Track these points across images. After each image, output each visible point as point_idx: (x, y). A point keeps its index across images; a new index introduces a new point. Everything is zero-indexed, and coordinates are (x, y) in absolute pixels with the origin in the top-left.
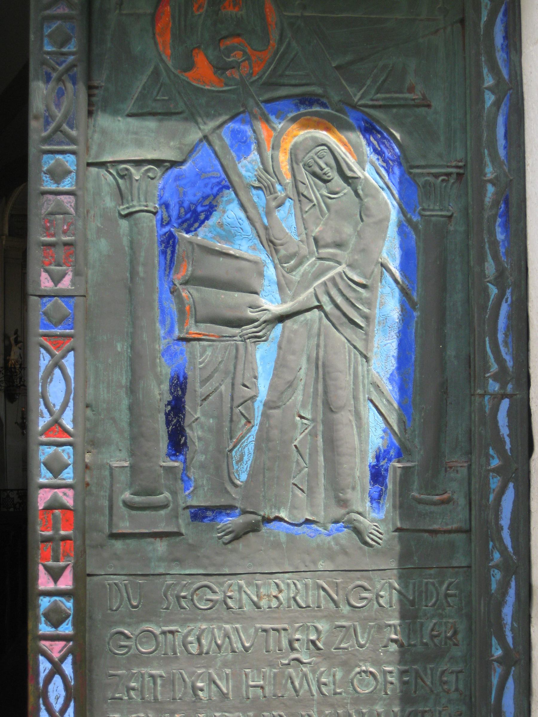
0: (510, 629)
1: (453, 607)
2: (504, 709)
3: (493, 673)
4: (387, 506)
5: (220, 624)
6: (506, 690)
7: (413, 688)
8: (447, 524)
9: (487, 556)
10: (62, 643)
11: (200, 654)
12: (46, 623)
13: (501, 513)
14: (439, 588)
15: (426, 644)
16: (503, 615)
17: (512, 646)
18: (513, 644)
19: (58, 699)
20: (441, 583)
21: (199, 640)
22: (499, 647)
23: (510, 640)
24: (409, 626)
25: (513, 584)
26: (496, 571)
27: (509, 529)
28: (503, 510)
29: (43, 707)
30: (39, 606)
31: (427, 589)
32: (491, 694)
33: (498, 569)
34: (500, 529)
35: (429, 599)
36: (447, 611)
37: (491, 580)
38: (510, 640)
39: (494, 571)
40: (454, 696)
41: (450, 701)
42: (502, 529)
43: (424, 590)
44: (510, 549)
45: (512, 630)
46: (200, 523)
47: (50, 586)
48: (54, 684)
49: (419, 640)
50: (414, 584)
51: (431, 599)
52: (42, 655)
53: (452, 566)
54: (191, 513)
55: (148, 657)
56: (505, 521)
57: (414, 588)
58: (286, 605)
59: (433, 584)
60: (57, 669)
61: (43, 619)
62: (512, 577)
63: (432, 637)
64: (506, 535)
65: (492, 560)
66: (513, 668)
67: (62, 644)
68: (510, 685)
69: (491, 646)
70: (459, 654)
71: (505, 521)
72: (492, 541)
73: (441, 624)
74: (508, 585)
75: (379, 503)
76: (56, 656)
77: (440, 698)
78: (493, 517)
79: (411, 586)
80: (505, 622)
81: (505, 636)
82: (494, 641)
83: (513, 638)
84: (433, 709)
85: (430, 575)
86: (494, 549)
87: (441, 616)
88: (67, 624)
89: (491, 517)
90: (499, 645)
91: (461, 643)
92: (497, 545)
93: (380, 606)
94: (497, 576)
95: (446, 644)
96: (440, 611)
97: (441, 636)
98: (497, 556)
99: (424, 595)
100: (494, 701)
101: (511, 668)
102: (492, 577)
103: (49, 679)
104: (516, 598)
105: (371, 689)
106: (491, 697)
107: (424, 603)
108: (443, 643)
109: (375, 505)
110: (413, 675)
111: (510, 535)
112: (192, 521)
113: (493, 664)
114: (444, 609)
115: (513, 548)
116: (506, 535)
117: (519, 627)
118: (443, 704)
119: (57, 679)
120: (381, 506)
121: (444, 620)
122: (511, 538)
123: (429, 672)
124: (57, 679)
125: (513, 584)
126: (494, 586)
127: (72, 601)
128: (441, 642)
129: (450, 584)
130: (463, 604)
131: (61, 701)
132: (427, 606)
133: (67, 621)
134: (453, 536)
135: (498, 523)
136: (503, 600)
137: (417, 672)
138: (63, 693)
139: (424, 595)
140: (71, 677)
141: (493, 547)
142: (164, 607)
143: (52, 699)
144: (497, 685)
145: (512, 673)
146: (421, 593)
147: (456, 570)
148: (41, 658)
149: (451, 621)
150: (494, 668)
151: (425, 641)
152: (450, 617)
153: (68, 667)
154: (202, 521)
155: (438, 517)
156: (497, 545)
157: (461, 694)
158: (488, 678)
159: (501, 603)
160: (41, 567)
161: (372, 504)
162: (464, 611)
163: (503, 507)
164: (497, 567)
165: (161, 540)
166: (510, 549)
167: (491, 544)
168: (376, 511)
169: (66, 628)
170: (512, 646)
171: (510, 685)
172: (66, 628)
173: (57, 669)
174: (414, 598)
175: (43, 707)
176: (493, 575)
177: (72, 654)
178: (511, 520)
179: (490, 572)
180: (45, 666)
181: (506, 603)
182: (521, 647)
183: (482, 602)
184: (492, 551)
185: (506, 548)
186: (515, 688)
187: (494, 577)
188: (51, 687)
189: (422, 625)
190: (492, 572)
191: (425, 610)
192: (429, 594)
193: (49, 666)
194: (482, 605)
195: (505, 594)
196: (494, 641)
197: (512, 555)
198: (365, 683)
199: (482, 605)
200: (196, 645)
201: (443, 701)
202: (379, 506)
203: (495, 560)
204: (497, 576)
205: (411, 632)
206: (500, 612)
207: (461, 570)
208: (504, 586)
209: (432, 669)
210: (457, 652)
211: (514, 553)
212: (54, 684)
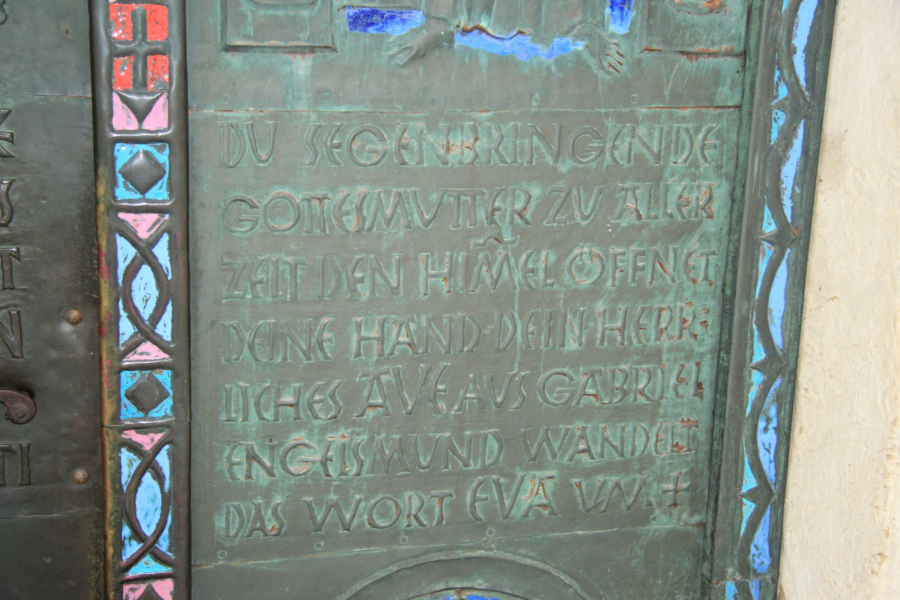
0: (789, 196)
1: (709, 163)
2: (771, 305)
3: (761, 257)
4: (634, 14)
5: (388, 188)
6: (776, 280)
7: (649, 277)
8: (713, 44)
9: (770, 91)
10: (154, 217)
11: (359, 231)
12: (126, 187)
13: (797, 27)
14: (693, 136)
15: (671, 216)
16: (782, 177)
17: (789, 220)
18: (792, 217)
19: (147, 300)
20: (698, 130)
21: (359, 209)
22: (772, 222)
23: (788, 212)
24: (651, 190)
25: (800, 132)
26: (780, 113)
27: (804, 52)
28: (799, 24)
29: (123, 314)
30: (113, 160)
31: (678, 138)
32: (756, 285)
33: (783, 111)
34: (792, 51)
35: (679, 152)
36: (702, 170)
37: (771, 126)
38: (788, 212)
39: (776, 114)
40: (702, 286)
41: (695, 294)
42: (795, 52)
43: (674, 140)
44: (803, 82)
45: (792, 197)
46: (362, 33)
47: (132, 124)
48: (141, 278)
49: (661, 210)
50: (661, 130)
51: (682, 153)
52: (122, 234)
53: (714, 105)
54: (349, 17)
55: (284, 236)
56: (800, 40)
57: (661, 135)
58: (484, 160)
59: (687, 130)
60: (145, 255)
61: (121, 179)
62: (800, 123)
63: (679, 207)
64: (799, 61)
65: (777, 97)
66: (788, 250)
67: (153, 217)
68: (782, 272)
69: (762, 219)
70: (713, 229)
71: (800, 40)
72: (780, 69)
73: (692, 189)
74: (794, 130)
75: (622, 9)
76: (144, 234)
77: (683, 290)
78: (785, 33)
79: (657, 134)
80: (784, 186)
81: (782, 205)
82: (767, 212)
83: (793, 208)
84: (672, 306)
85: (684, 118)
86: (780, 80)
87: (694, 177)
88: (160, 188)
89: (783, 33)
90: (773, 217)
91: (716, 214)
92: (786, 76)
93: (614, 159)
94: (780, 119)
95: (697, 215)
96: (693, 169)
97: (691, 205)
98: (783, 92)
99: (673, 146)
100: (760, 295)
101: (786, 250)
102: (773, 122)
103: (132, 271)
104: (802, 153)
105: (595, 277)
106: (755, 289)
107: (672, 159)
108: (693, 215)
109: (617, 12)
110: (651, 258)
111: (805, 61)
112: (351, 29)
113: (763, 245)
114: (698, 167)
115: (806, 80)
116: (799, 61)
117: (802, 193)
118: (687, 299)
119: (146, 272)
120: (624, 13)
121: (697, 183)
122: (805, 65)
123: (671, 255)
124: (146, 272)
125: (800, 132)
126: (774, 135)
127: (167, 151)
128: (690, 212)
129: (709, 131)
130: (724, 160)
131: (152, 304)
132: (675, 163)
133: (160, 183)
134: (720, 60)
135: (791, 43)
136: (785, 156)
137: (657, 255)
138: (154, 293)
139: (673, 146)
140: (167, 268)
141: (779, 79)
142: (307, 162)
143: (138, 302)
144: (766, 273)
145: (786, 256)
146: (668, 146)
147: (719, 110)
148: (121, 242)
149: (706, 183)
150: (764, 249)
151: (669, 211)
152: (705, 177)
153: (161, 251)
154: (365, 31)
155: (702, 32)
156: (786, 76)
157: (711, 285)
158: (753, 262)
159: (780, 161)
160: (116, 98)
161: (613, 10)
162: (724, 170)
163: (800, 18)
164: (781, 106)
165: (303, 58)
166: (803, 82)
167: (777, 73)
168: (619, 21)
169: (159, 193)
170: (789, 220)
171: (782, 272)
172: (159, 193)
173: (145, 255)
174: (660, 151)
175: (123, 314)
176: (775, 119)
177: (170, 233)
178: (809, 38)
179: (771, 114)
180: (126, 252)
181: (788, 159)
182: (801, 222)
183: (757, 158)
184: (778, 85)
185: (797, 80)
186: (788, 278)
187: (776, 122)
188: (136, 284)
189: (667, 188)
190: (774, 115)
191: (673, 168)
192: (680, 145)
193: (132, 252)
194: (756, 162)
195: (788, 145)
196: (767, 212)
197: (804, 89)
198: (586, 270)
199: (756, 162)
200: (353, 218)
201: (688, 294)
202: (622, 14)
203: (780, 98)
204: (780, 119)
205: (652, 198)
206: (780, 171)
207: (726, 111)
208: (787, 137)
209: (675, 250)
210: (710, 227)
211: (807, 88)
212: (141, 278)
